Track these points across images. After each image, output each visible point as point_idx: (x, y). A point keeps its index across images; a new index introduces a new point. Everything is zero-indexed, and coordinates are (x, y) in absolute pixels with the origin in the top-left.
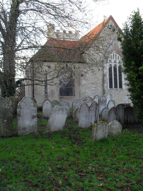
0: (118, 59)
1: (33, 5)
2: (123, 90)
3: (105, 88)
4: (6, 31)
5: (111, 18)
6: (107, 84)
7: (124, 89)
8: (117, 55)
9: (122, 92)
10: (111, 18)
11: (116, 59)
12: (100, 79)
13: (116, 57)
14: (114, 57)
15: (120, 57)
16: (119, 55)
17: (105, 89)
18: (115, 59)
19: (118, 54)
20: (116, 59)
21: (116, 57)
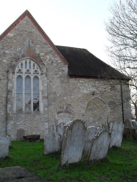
0: (34, 68)
1: (133, 58)
2: (39, 114)
3: (8, 110)
4: (67, 129)
5: (27, 14)
6: (12, 105)
7: (41, 112)
8: (32, 63)
9: (37, 117)
10: (27, 14)
11: (30, 68)
12: (2, 97)
13: (30, 66)
14: (26, 66)
15: (36, 64)
16: (35, 62)
17: (8, 112)
18: (28, 68)
19: (33, 60)
20: (30, 68)
21: (30, 66)
